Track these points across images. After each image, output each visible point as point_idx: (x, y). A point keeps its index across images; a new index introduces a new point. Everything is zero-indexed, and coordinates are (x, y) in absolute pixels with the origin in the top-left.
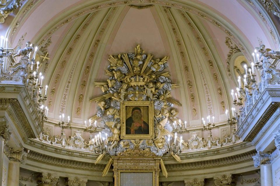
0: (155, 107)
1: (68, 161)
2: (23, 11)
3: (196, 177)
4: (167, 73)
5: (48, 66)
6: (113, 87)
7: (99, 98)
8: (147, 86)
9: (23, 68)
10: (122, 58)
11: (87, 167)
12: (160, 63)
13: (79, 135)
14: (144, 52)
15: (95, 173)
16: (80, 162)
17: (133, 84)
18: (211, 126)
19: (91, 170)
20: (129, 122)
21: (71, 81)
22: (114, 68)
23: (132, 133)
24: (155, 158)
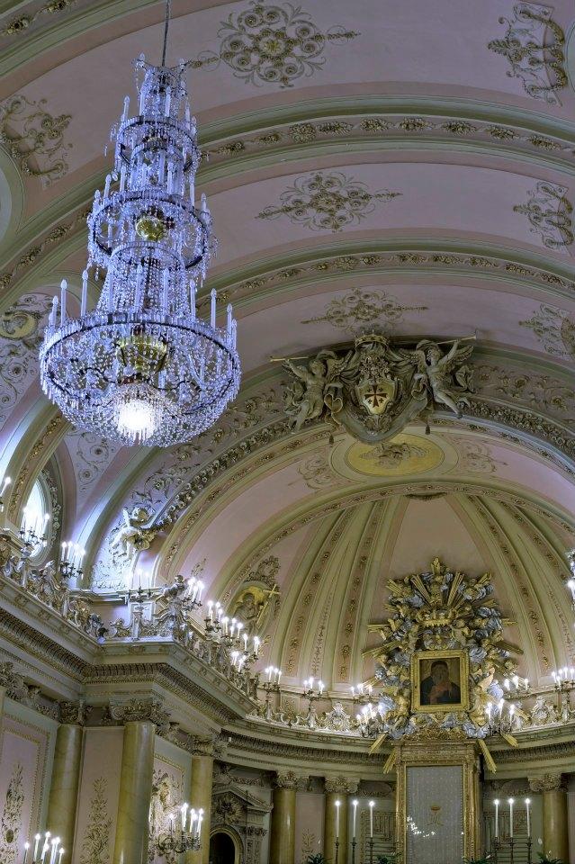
0: (472, 659)
1: (323, 751)
2: (181, 526)
3: (547, 770)
4: (492, 601)
5: (281, 605)
6: (401, 631)
7: (378, 650)
8: (455, 626)
9: (172, 616)
10: (411, 583)
11: (359, 760)
12: (477, 586)
13: (339, 709)
14: (448, 570)
15: (373, 769)
16: (346, 753)
17: (429, 623)
18: (570, 686)
19: (367, 765)
20: (426, 686)
21: (326, 625)
22: (400, 600)
23: (432, 702)
24: (465, 741)
